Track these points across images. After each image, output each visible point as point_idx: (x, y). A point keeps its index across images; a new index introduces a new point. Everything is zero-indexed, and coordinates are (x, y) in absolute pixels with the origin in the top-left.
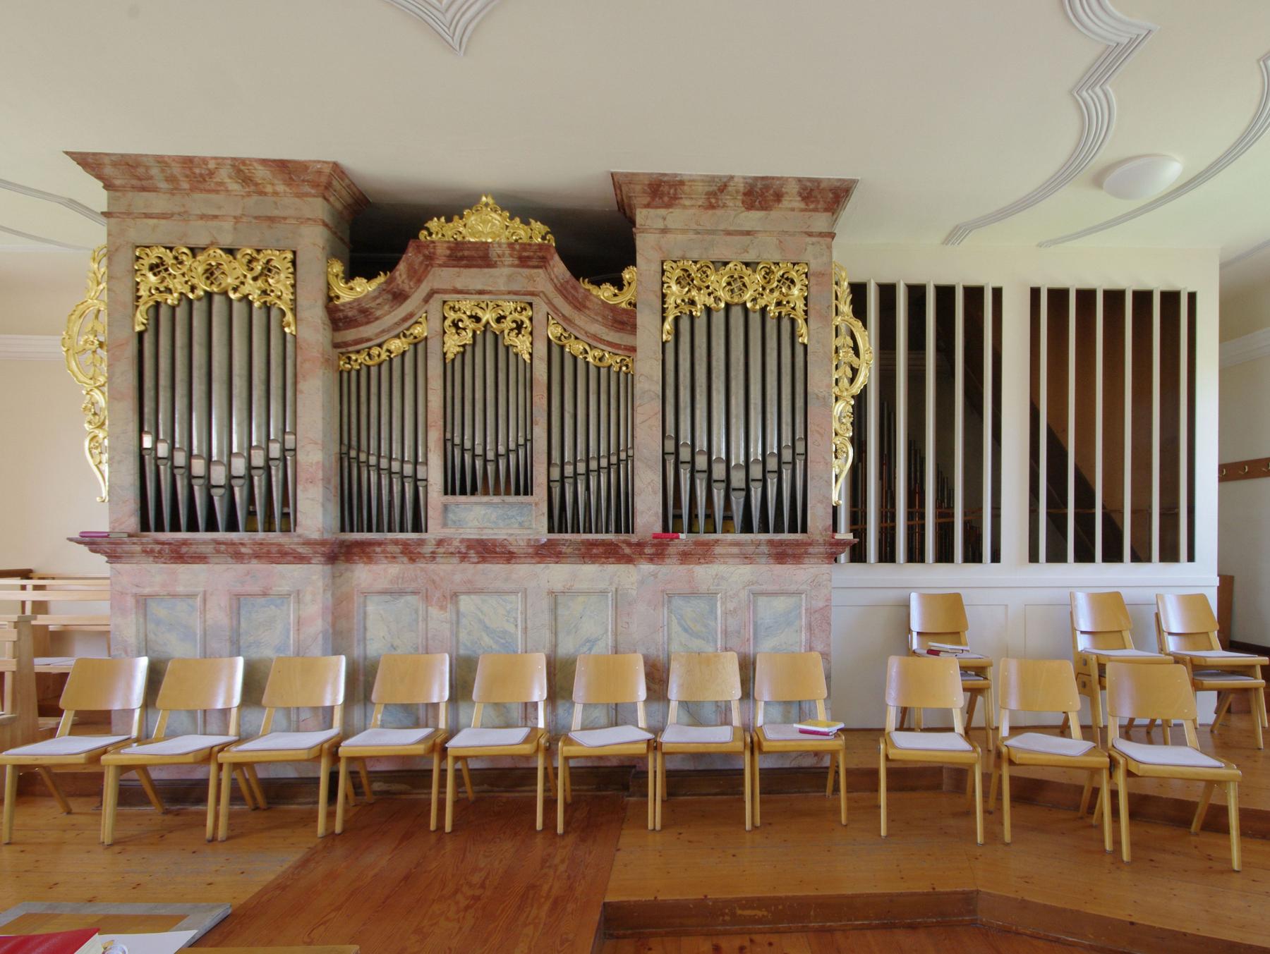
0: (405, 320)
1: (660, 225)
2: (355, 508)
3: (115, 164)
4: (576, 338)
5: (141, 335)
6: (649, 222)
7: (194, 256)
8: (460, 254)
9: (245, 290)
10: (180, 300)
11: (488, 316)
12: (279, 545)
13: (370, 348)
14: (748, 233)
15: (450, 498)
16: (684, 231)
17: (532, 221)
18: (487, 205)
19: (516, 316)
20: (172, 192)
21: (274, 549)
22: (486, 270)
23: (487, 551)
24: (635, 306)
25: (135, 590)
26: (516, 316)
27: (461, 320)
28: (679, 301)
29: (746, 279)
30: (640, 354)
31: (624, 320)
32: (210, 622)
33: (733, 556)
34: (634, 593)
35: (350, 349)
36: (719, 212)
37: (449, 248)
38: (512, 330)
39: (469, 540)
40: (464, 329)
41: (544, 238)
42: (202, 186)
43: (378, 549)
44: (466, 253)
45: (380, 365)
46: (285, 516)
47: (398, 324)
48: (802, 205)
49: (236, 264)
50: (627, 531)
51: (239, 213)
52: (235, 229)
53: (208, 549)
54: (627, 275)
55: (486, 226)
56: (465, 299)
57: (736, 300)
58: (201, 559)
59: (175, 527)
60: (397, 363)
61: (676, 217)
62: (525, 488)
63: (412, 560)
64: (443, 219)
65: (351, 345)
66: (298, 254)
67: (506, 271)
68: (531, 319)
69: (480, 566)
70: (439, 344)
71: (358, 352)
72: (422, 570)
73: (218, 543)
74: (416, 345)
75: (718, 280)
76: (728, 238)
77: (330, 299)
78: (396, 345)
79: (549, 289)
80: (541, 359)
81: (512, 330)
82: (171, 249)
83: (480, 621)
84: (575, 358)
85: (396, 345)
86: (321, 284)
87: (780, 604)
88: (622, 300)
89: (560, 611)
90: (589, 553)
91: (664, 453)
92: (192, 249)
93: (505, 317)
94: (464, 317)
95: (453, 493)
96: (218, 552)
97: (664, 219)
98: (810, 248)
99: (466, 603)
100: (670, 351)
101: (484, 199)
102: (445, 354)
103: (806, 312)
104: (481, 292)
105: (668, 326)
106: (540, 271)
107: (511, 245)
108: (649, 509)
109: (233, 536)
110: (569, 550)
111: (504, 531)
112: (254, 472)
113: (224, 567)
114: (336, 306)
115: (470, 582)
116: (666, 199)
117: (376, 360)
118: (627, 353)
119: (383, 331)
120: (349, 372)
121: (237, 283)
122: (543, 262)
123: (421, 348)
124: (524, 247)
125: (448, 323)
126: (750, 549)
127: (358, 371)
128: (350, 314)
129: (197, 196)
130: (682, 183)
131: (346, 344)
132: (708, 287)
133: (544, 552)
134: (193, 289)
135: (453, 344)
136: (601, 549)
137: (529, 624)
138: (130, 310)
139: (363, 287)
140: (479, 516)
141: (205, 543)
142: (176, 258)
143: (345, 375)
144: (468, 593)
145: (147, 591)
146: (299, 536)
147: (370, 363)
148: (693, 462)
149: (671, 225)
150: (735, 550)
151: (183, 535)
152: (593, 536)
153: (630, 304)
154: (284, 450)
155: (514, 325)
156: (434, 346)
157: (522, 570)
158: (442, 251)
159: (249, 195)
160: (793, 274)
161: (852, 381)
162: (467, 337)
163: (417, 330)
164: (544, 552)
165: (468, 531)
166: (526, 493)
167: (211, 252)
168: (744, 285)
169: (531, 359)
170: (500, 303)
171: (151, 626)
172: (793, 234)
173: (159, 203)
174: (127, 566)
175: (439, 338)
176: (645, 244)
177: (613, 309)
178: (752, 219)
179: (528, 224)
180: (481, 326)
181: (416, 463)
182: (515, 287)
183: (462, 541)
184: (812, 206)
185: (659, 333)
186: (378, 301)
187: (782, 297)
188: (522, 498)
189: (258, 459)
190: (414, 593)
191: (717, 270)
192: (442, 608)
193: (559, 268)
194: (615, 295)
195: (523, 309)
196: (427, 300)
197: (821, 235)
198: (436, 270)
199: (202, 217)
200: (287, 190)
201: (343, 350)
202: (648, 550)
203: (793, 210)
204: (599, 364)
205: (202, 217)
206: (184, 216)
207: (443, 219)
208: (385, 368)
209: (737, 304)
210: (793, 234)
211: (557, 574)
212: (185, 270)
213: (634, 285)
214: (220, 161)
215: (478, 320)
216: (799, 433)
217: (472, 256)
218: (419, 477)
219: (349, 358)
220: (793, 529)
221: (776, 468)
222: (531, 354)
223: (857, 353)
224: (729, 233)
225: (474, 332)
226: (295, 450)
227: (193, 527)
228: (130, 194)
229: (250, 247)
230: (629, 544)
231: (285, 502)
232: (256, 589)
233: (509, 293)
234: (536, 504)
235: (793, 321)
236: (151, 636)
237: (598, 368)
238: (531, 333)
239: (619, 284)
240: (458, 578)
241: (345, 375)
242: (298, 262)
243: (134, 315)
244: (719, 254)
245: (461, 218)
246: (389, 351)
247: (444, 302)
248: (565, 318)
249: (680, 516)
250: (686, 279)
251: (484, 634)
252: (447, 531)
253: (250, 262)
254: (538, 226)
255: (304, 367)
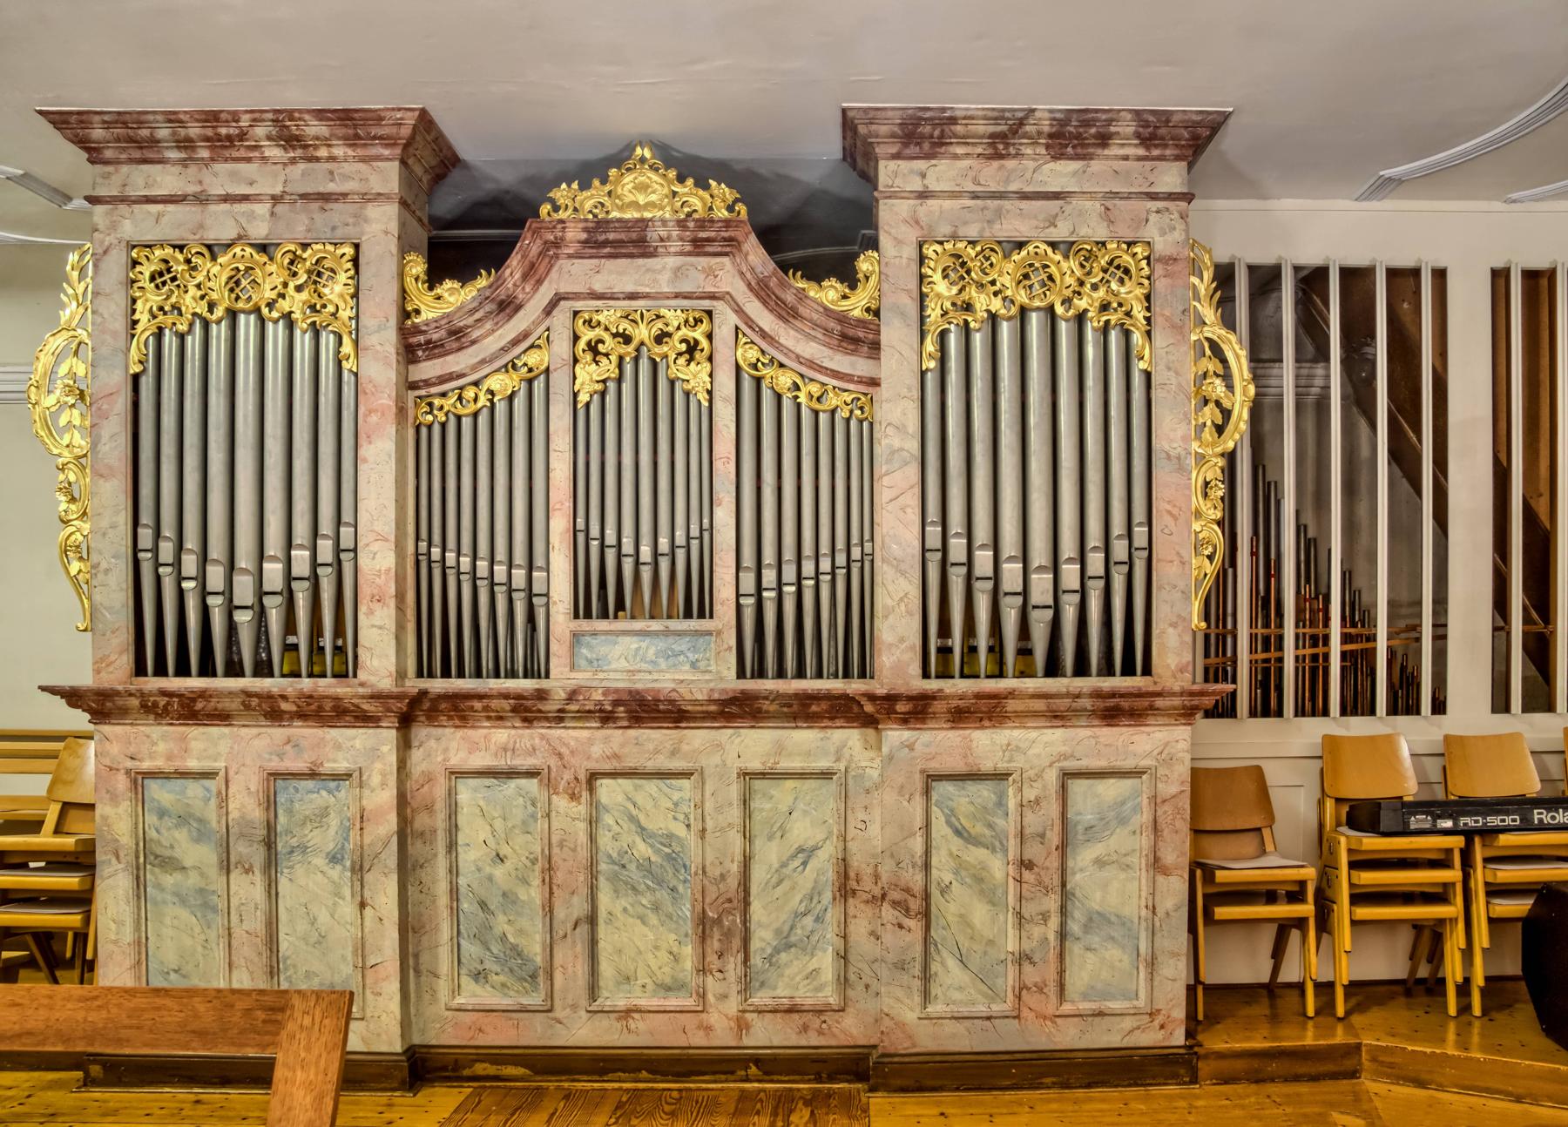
0: (515, 342)
1: (916, 185)
2: (442, 639)
3: (107, 125)
4: (781, 365)
5: (136, 378)
6: (898, 182)
7: (214, 258)
8: (602, 238)
9: (284, 305)
10: (191, 325)
11: (642, 333)
12: (337, 699)
13: (461, 388)
14: (1056, 196)
15: (584, 625)
16: (954, 195)
17: (713, 183)
18: (643, 160)
19: (684, 332)
20: (184, 163)
21: (328, 705)
22: (641, 261)
23: (643, 709)
24: (877, 313)
25: (129, 764)
26: (684, 332)
27: (603, 342)
28: (948, 305)
29: (1053, 269)
30: (884, 392)
31: (860, 337)
32: (234, 815)
33: (1035, 714)
34: (875, 774)
35: (434, 390)
36: (1010, 164)
37: (585, 230)
38: (680, 354)
39: (617, 691)
40: (607, 355)
41: (730, 209)
42: (227, 153)
43: (478, 705)
44: (611, 236)
45: (475, 415)
46: (339, 650)
47: (504, 350)
48: (1141, 152)
49: (272, 268)
50: (862, 675)
51: (278, 190)
52: (272, 214)
53: (233, 705)
54: (864, 264)
55: (644, 194)
56: (608, 308)
57: (1037, 303)
58: (223, 718)
59: (183, 670)
60: (501, 408)
61: (942, 173)
62: (698, 605)
63: (528, 721)
64: (575, 186)
65: (434, 384)
66: (363, 249)
67: (672, 262)
68: (710, 337)
69: (632, 733)
70: (567, 379)
71: (444, 395)
72: (542, 737)
73: (248, 694)
74: (530, 382)
75: (1006, 273)
76: (1025, 204)
77: (405, 315)
78: (501, 383)
79: (739, 290)
80: (725, 400)
81: (680, 354)
82: (181, 248)
83: (633, 819)
84: (779, 397)
85: (501, 383)
86: (392, 293)
87: (1110, 789)
88: (856, 306)
89: (756, 804)
90: (803, 710)
91: (924, 550)
92: (209, 247)
93: (669, 335)
94: (606, 337)
95: (588, 615)
96: (247, 707)
97: (923, 176)
98: (1153, 218)
99: (608, 790)
100: (932, 385)
101: (639, 151)
102: (575, 395)
103: (1148, 319)
104: (632, 296)
105: (930, 346)
106: (726, 260)
107: (681, 224)
108: (902, 640)
109: (264, 684)
110: (773, 708)
111: (668, 676)
112: (295, 585)
113: (255, 731)
114: (415, 326)
115: (616, 756)
116: (926, 146)
117: (472, 408)
118: (862, 388)
119: (483, 362)
120: (430, 427)
121: (273, 295)
122: (731, 246)
123: (538, 386)
124: (702, 224)
125: (582, 344)
126: (1063, 704)
127: (443, 426)
128: (435, 337)
129: (219, 167)
130: (953, 120)
131: (427, 383)
132: (993, 283)
133: (734, 709)
134: (211, 307)
135: (589, 375)
136: (824, 705)
137: (710, 824)
138: (122, 343)
139: (455, 296)
140: (627, 655)
141: (231, 694)
142: (188, 261)
143: (424, 431)
144: (613, 775)
145: (146, 765)
146: (362, 685)
147: (461, 411)
148: (970, 563)
149: (934, 186)
150: (1040, 705)
151: (195, 683)
152: (810, 685)
153: (868, 310)
154: (338, 551)
155: (684, 347)
156: (560, 381)
157: (697, 739)
158: (574, 234)
159: (293, 161)
160: (1127, 259)
161: (1220, 430)
162: (608, 368)
163: (533, 359)
164: (734, 709)
165: (612, 675)
166: (701, 615)
167: (237, 250)
168: (1051, 278)
169: (711, 401)
170: (663, 312)
171: (151, 819)
172: (1128, 197)
173: (167, 179)
174: (118, 729)
175: (567, 370)
176: (894, 218)
177: (842, 318)
178: (1060, 174)
179: (707, 187)
180: (631, 348)
181: (530, 568)
182: (687, 287)
183: (607, 692)
184: (1156, 152)
185: (916, 357)
186: (477, 316)
187: (1110, 298)
188: (694, 624)
189: (301, 565)
190: (531, 774)
191: (1007, 256)
192: (573, 797)
193: (756, 255)
194: (845, 297)
195: (698, 321)
196: (549, 310)
197: (1171, 197)
198: (563, 263)
199: (227, 199)
200: (350, 152)
201: (423, 392)
202: (901, 707)
203: (1126, 158)
204: (817, 406)
205: (227, 199)
206: (201, 199)
207: (575, 186)
208: (483, 420)
209: (1038, 309)
210: (1128, 197)
211: (752, 745)
212: (200, 278)
213: (873, 280)
214: (257, 116)
215: (627, 339)
216: (1139, 514)
217: (625, 241)
218: (536, 590)
219: (430, 405)
220: (1129, 670)
221: (1101, 572)
222: (710, 392)
223: (1230, 387)
224: (1024, 196)
225: (621, 359)
226: (355, 550)
227: (207, 669)
228: (125, 169)
229: (291, 241)
230: (872, 698)
231: (339, 631)
232: (300, 765)
233: (677, 296)
234: (719, 633)
235: (1127, 334)
236: (152, 834)
237: (816, 413)
238: (710, 359)
239: (850, 279)
240: (597, 750)
241: (424, 431)
242: (362, 260)
243: (128, 349)
244: (1012, 227)
245: (604, 181)
246: (492, 393)
247: (576, 313)
248: (764, 334)
249: (950, 650)
250: (959, 268)
251: (638, 840)
252: (579, 675)
253: (292, 262)
254: (723, 192)
255: (369, 421)
